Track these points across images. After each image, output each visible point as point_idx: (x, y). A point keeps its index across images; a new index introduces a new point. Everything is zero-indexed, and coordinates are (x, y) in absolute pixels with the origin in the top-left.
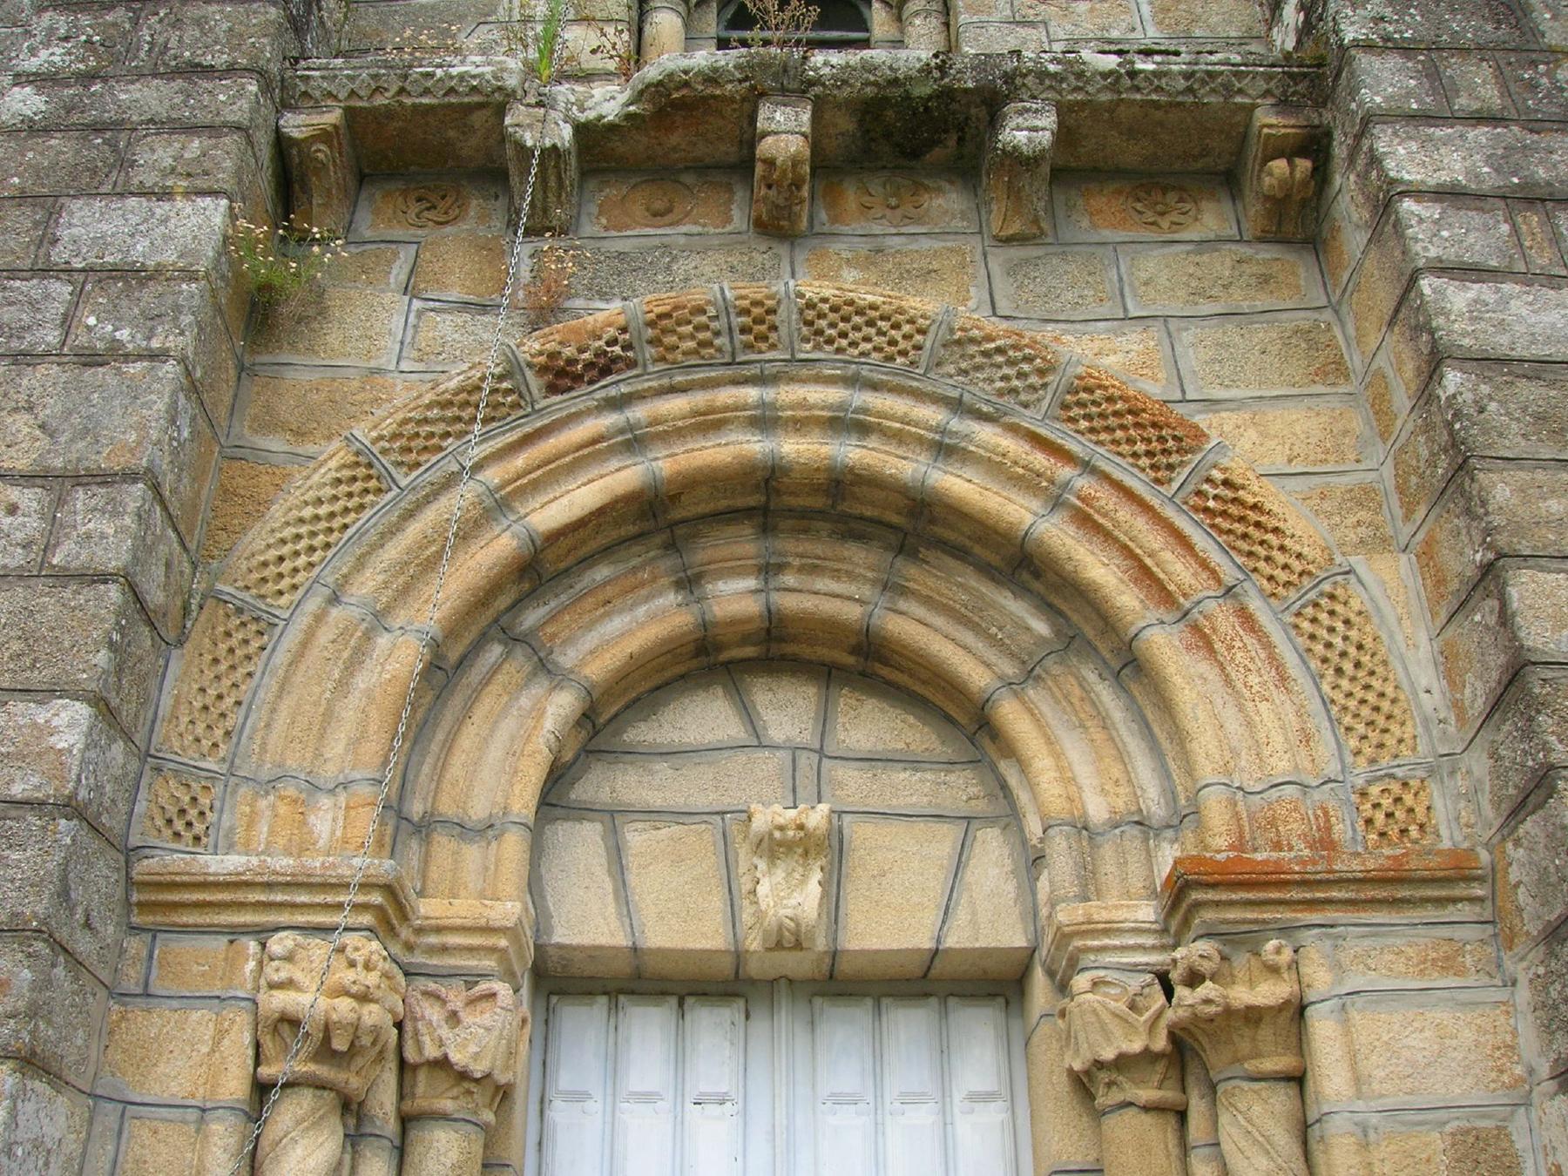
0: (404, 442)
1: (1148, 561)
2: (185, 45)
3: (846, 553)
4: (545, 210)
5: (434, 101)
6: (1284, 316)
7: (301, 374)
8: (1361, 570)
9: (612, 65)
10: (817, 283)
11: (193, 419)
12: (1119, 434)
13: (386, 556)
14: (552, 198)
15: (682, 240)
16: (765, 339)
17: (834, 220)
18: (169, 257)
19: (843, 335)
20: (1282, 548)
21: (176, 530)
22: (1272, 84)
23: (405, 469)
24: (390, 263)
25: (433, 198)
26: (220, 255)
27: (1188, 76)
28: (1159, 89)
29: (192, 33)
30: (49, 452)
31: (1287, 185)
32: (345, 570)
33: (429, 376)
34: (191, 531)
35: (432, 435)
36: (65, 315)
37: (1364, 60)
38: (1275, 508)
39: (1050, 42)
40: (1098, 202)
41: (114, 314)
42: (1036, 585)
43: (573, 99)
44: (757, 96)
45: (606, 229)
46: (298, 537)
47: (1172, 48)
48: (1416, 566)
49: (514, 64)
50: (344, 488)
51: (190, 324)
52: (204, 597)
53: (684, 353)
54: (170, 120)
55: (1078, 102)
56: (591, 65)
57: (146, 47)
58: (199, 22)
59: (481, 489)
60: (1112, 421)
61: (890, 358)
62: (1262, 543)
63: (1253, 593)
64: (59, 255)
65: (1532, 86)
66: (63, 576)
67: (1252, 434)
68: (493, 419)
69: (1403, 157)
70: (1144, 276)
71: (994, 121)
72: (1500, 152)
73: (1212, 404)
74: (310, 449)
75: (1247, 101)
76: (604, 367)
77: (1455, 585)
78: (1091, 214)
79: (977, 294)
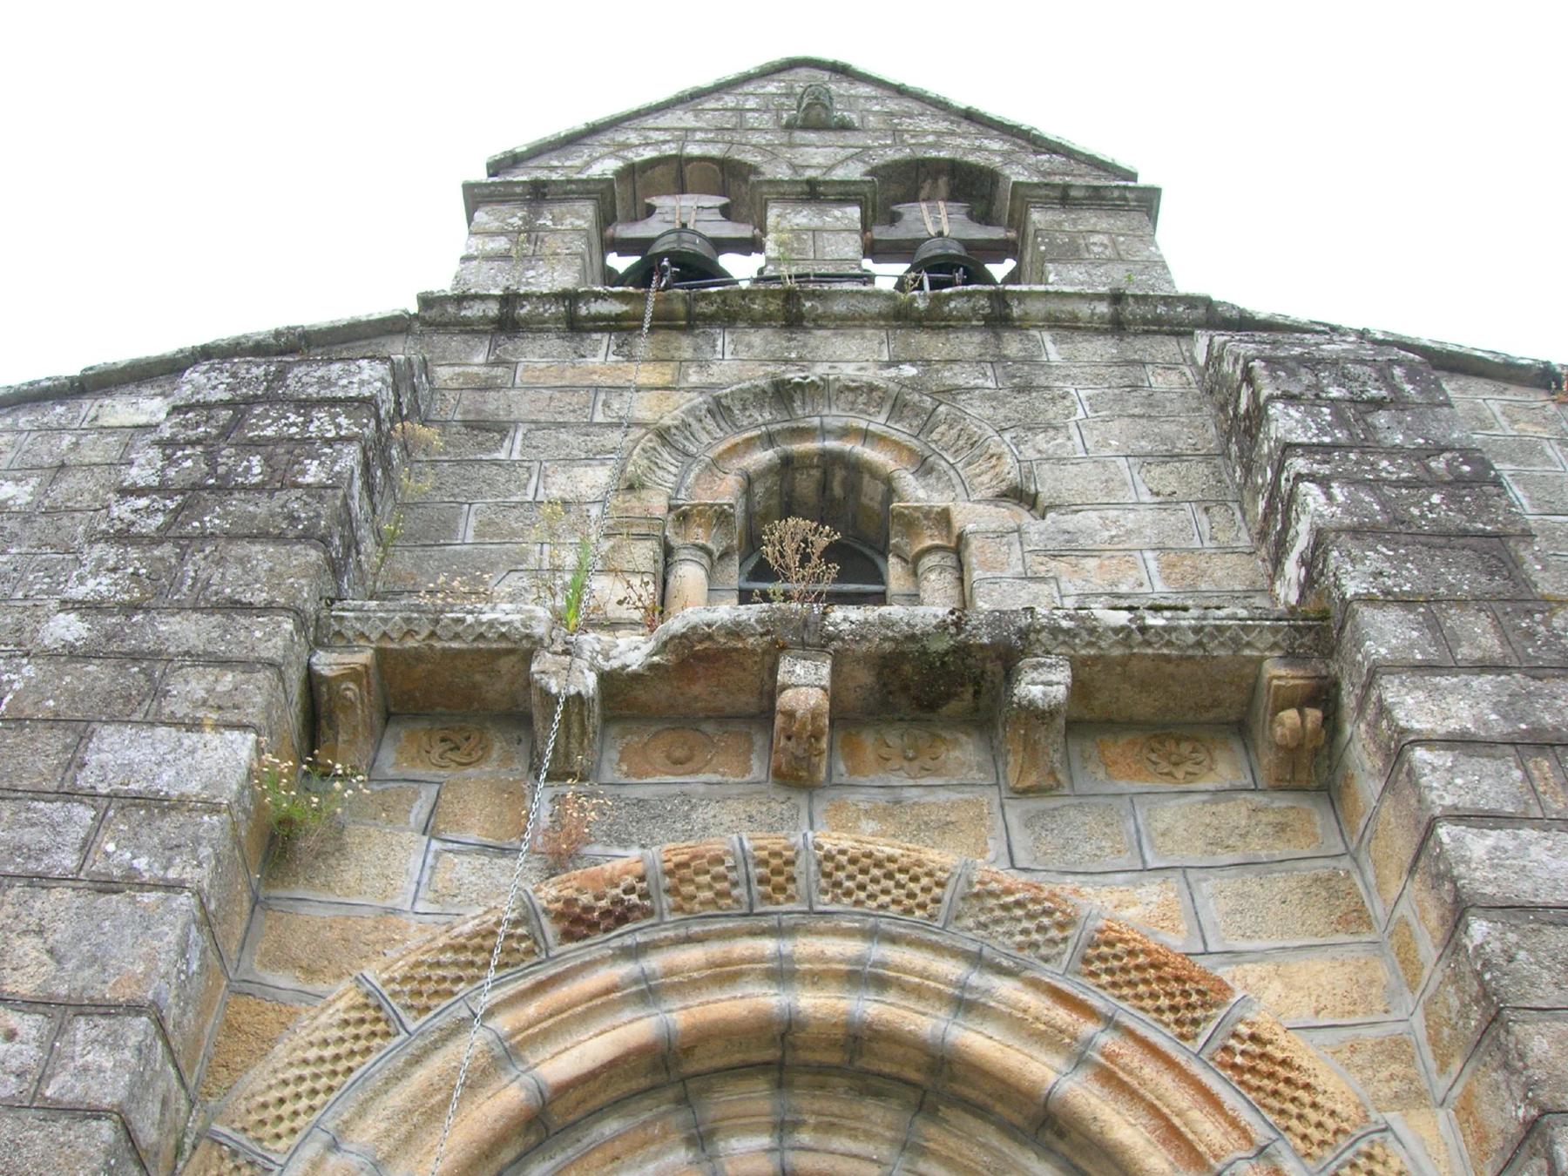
0: (415, 985)
1: (1176, 1121)
2: (227, 582)
3: (864, 1112)
4: (567, 755)
5: (464, 646)
6: (1303, 864)
7: (314, 908)
8: (1398, 1126)
9: (637, 615)
10: (835, 835)
11: (204, 952)
12: (1142, 988)
13: (390, 1103)
14: (574, 744)
15: (702, 789)
16: (783, 889)
17: (853, 771)
18: (193, 787)
19: (862, 887)
20: (1314, 1105)
21: (176, 1066)
22: (1279, 637)
23: (414, 1013)
24: (411, 802)
25: (458, 738)
26: (243, 787)
27: (1197, 630)
28: (1169, 644)
29: (234, 571)
30: (54, 978)
31: (1300, 732)
32: (346, 1116)
33: (442, 919)
34: (191, 1068)
35: (444, 979)
36: (85, 841)
37: (1366, 614)
38: (1305, 1064)
39: (1062, 597)
40: (1113, 752)
41: (133, 842)
42: (1062, 1147)
43: (598, 648)
44: (777, 649)
45: (627, 775)
46: (301, 1079)
47: (1179, 603)
48: (1455, 1122)
49: (542, 613)
50: (351, 1030)
51: (208, 857)
52: (199, 1136)
53: (701, 903)
54: (206, 653)
55: (1090, 657)
56: (617, 614)
57: (190, 582)
58: (241, 561)
59: (491, 1037)
60: (1134, 975)
61: (909, 911)
62: (1293, 1100)
63: (1286, 1153)
64: (86, 779)
65: (1530, 635)
66: (57, 1110)
67: (1277, 986)
68: (506, 965)
69: (1412, 707)
70: (1161, 826)
71: (1010, 675)
72: (1505, 699)
73: (1233, 955)
74: (319, 987)
75: (1256, 653)
76: (620, 915)
77: (1497, 1142)
78: (1107, 765)
79: (996, 847)
